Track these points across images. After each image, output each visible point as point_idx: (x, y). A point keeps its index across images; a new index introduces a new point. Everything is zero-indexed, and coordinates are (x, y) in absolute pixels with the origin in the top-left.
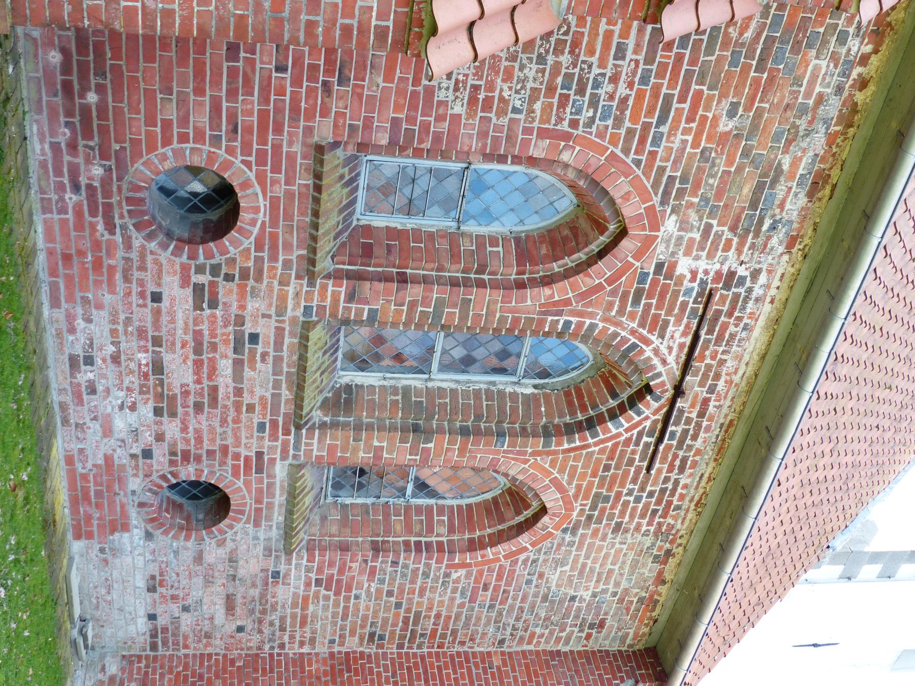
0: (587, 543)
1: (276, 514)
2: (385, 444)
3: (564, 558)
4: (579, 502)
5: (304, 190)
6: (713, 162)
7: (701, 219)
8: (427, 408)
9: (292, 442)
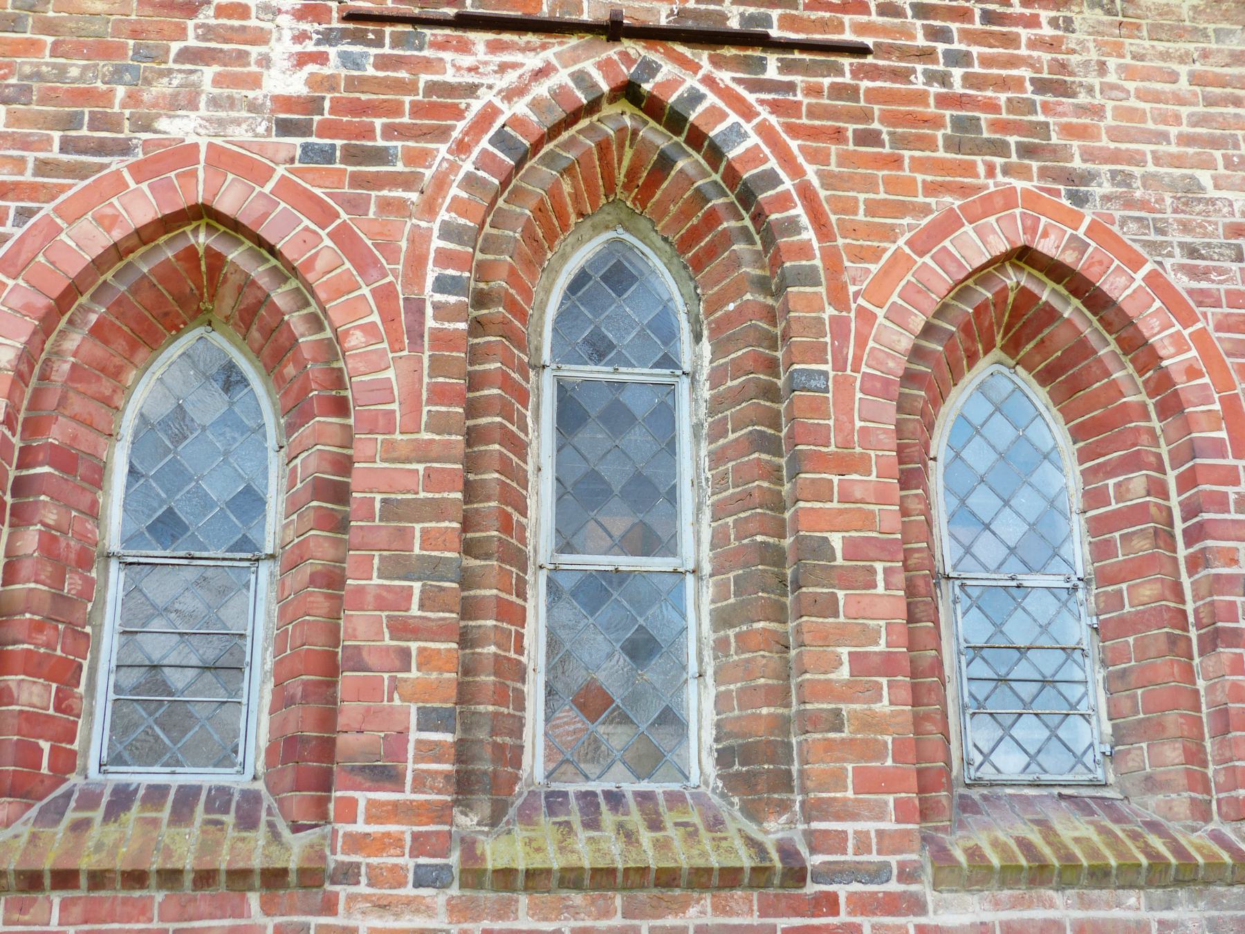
0: (1112, 145)
1: (1117, 913)
2: (844, 651)
3: (1172, 187)
4: (982, 180)
5: (77, 911)
6: (29, 77)
7: (170, 71)
8: (746, 565)
9: (856, 887)
